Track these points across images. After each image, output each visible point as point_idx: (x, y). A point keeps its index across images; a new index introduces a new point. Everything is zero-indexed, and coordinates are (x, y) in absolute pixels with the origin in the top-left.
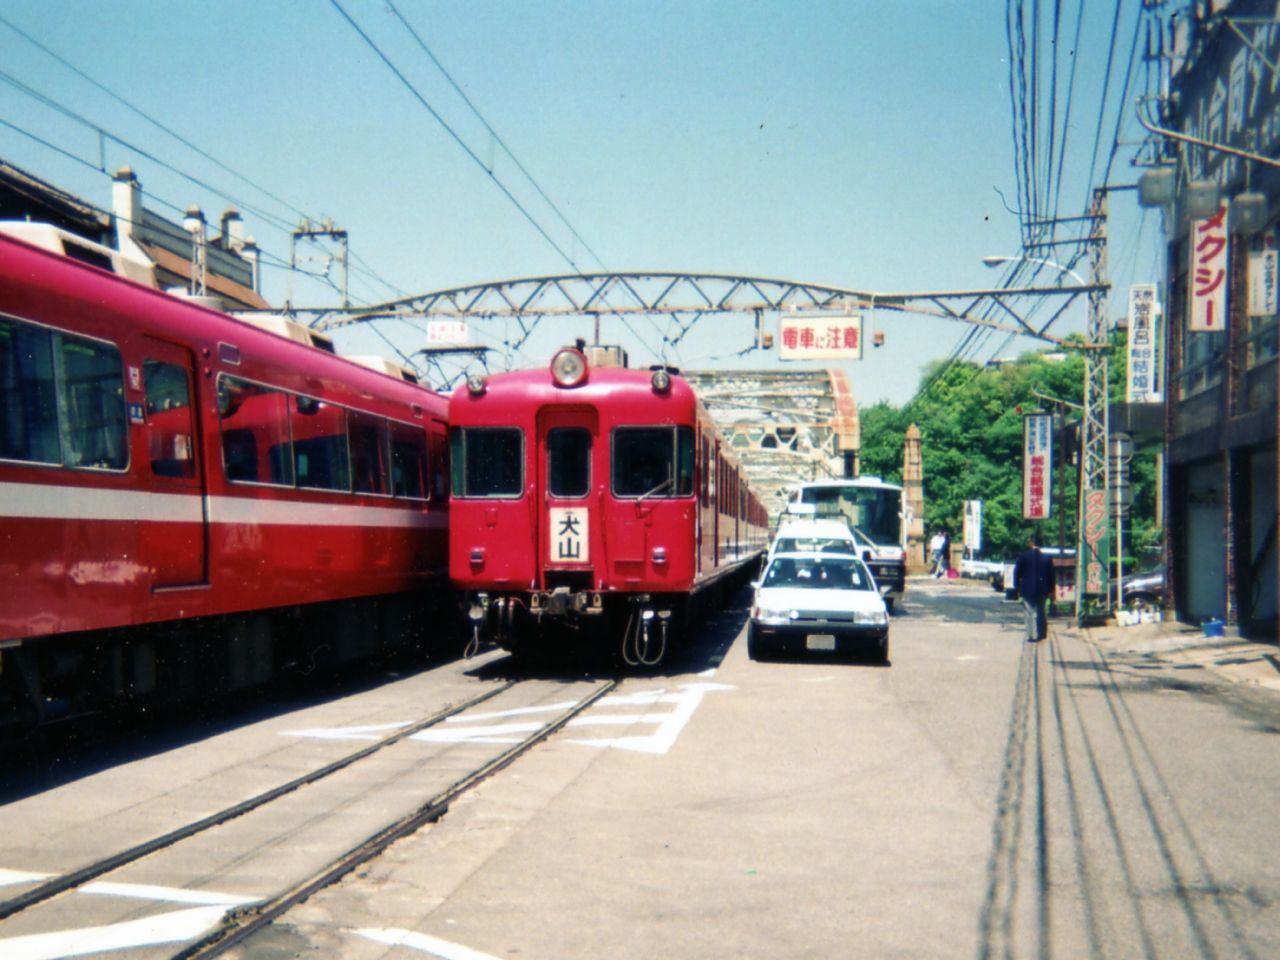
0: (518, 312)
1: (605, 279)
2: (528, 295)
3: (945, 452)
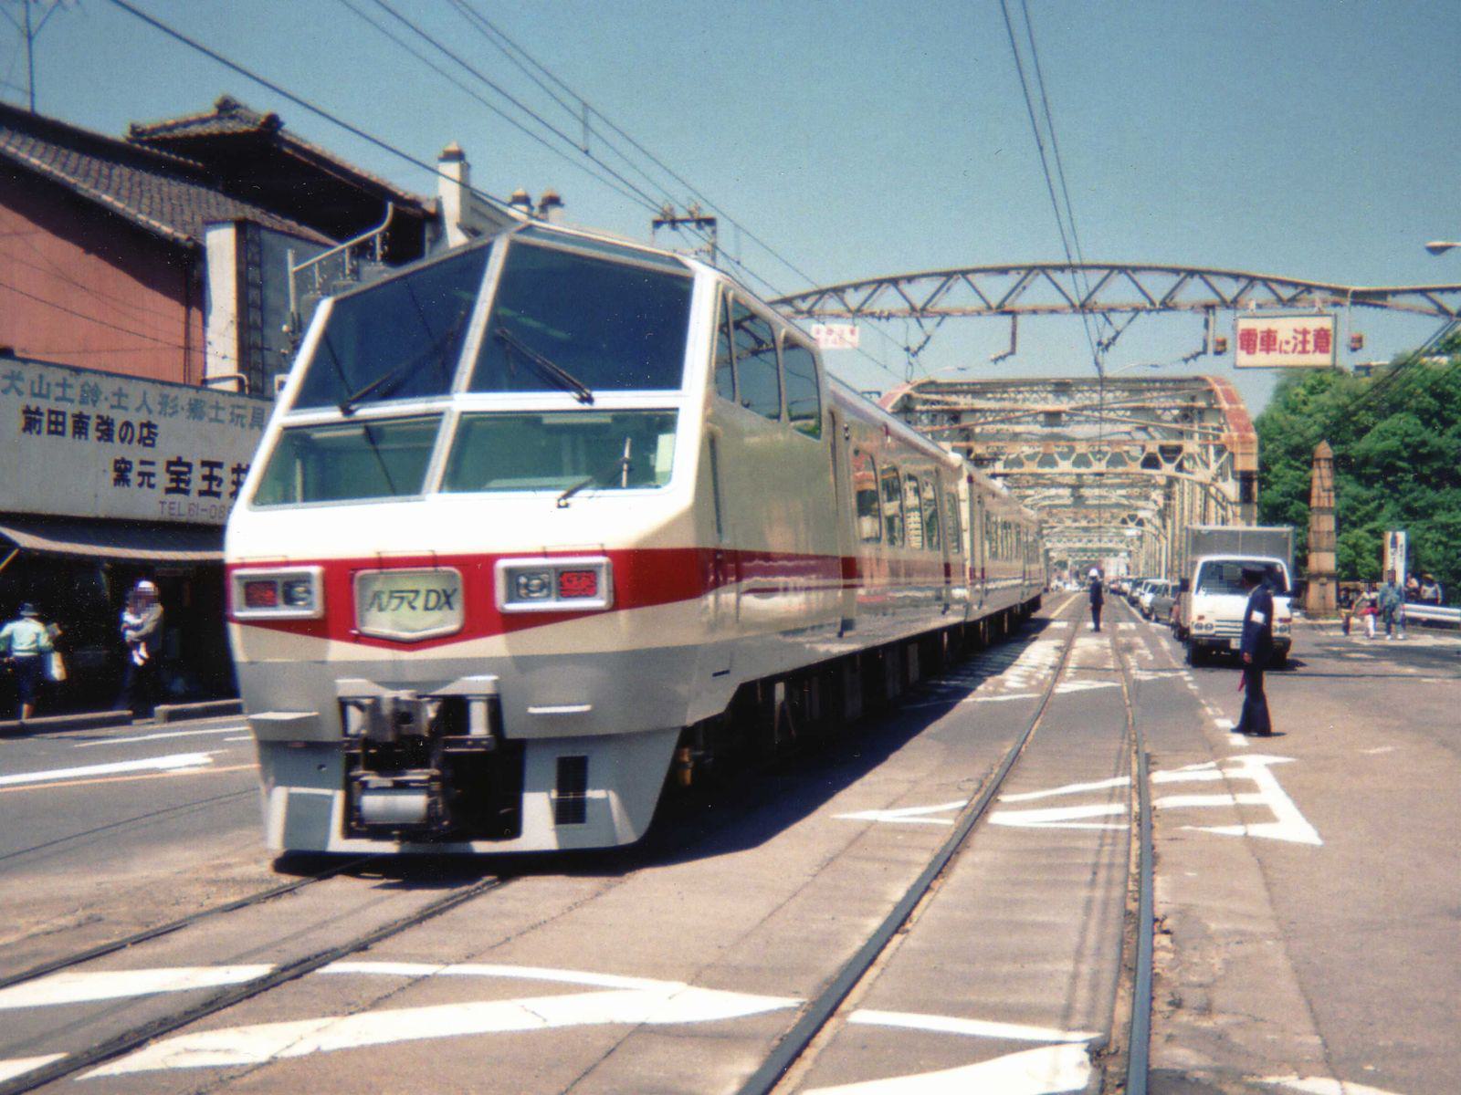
0: (918, 313)
1: (1023, 273)
2: (933, 290)
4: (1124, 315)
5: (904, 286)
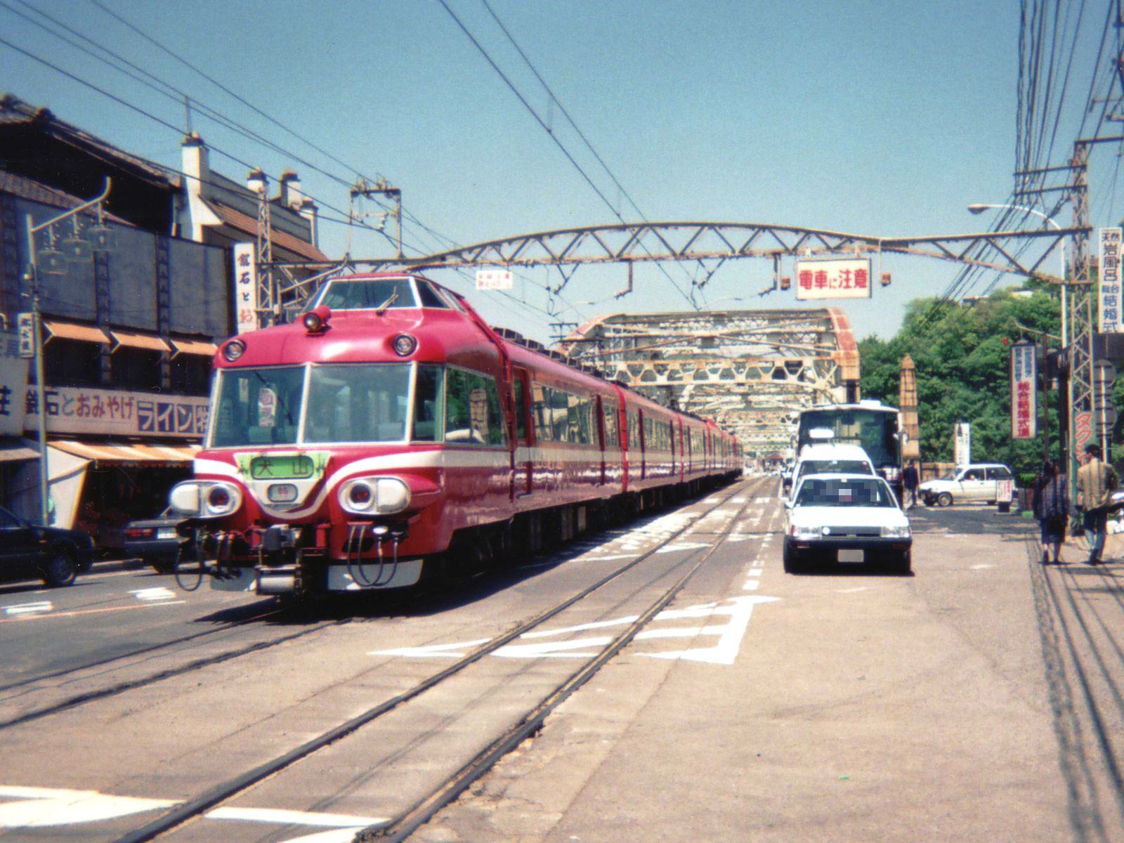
0: (558, 261)
3: (928, 380)
4: (715, 260)
5: (547, 241)
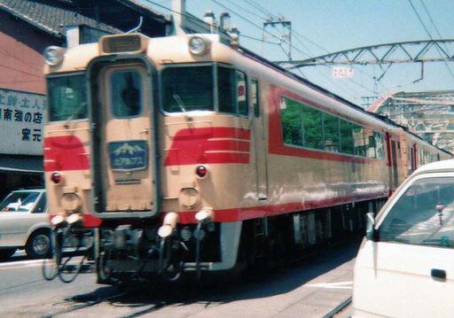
5: (374, 50)
